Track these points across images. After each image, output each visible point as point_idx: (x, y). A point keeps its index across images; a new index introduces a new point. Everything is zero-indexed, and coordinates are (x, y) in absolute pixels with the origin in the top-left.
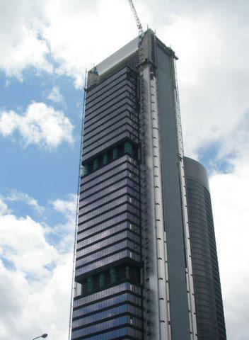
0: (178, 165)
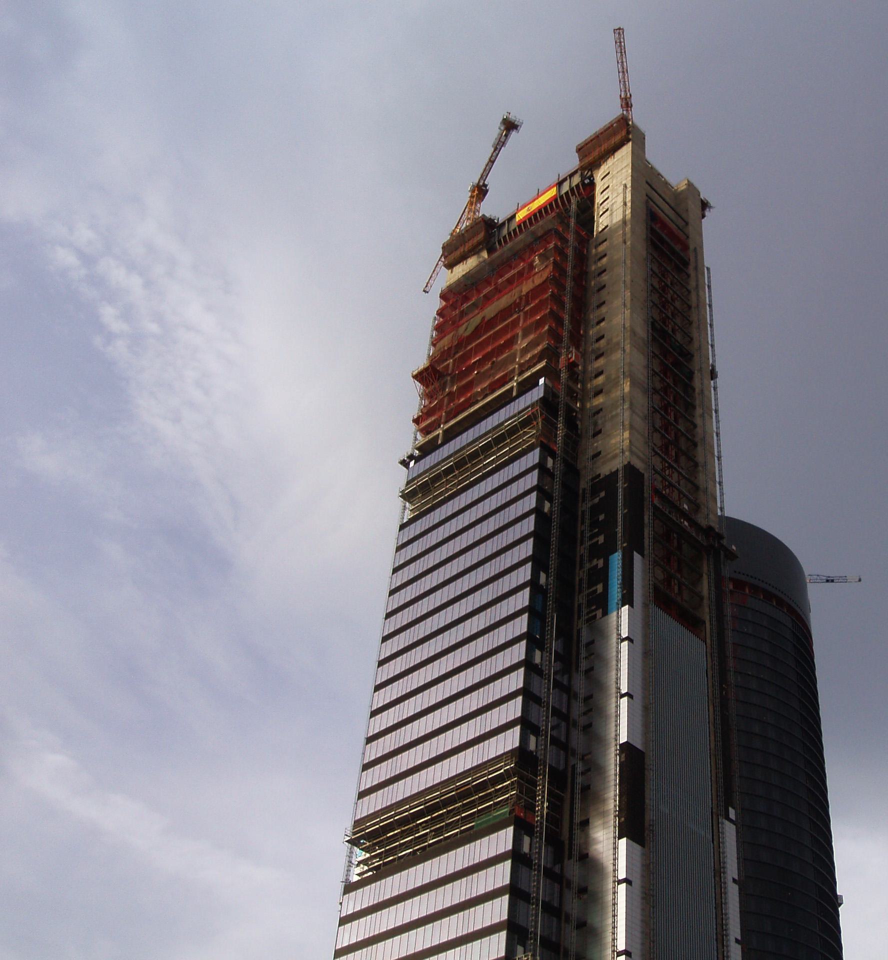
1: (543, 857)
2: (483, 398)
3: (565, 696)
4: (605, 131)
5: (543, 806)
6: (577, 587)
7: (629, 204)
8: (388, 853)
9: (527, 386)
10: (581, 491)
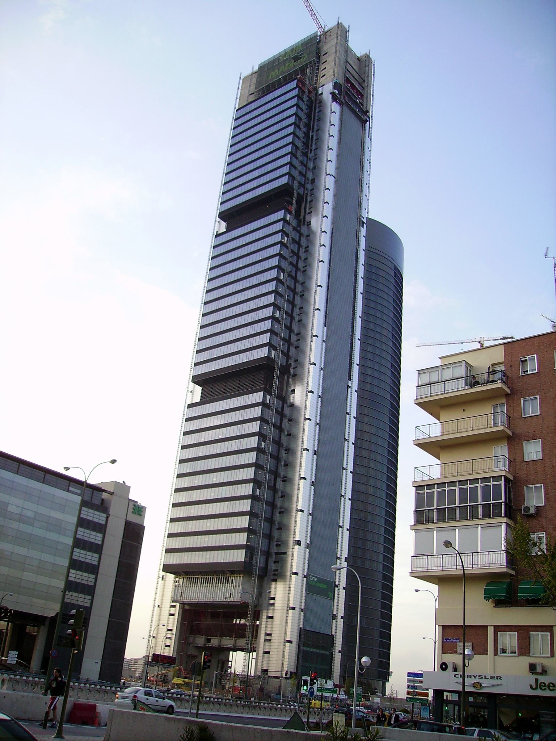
0: (358, 232)
3: (305, 168)
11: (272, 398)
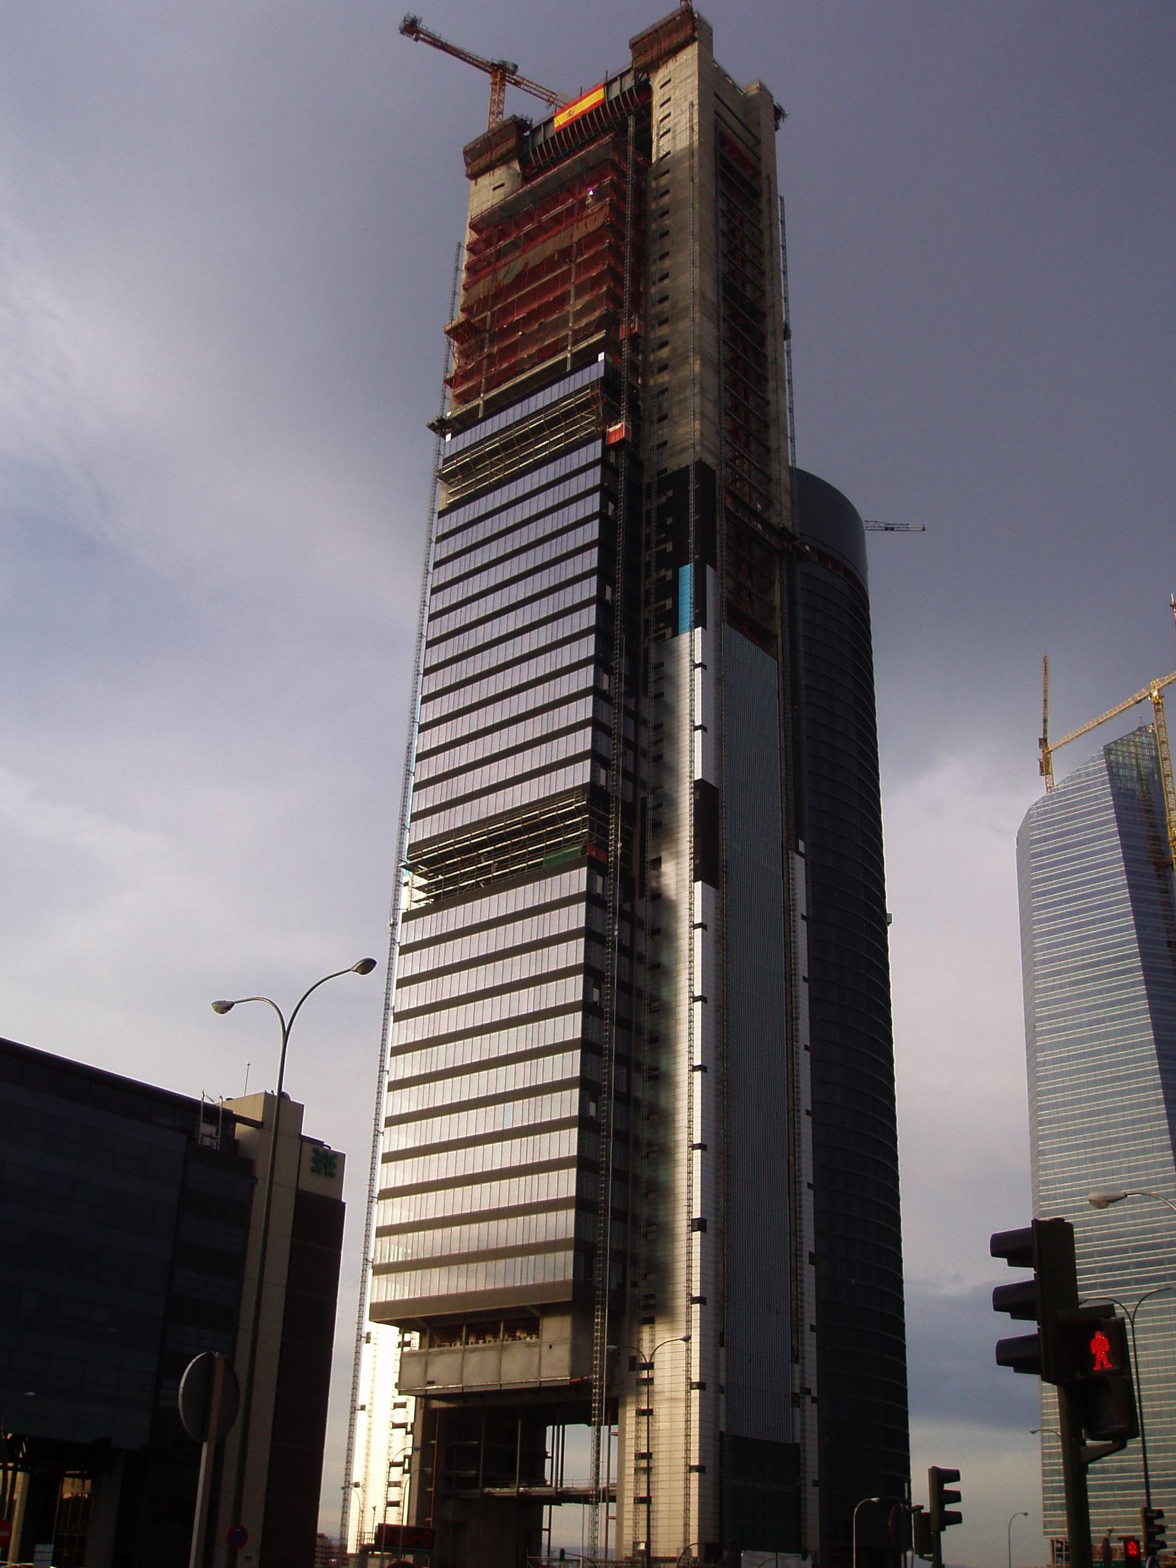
1: (615, 896)
2: (529, 369)
4: (666, 24)
5: (616, 846)
6: (643, 599)
7: (696, 128)
8: (448, 882)
9: (585, 359)
10: (645, 487)
11: (613, 681)
